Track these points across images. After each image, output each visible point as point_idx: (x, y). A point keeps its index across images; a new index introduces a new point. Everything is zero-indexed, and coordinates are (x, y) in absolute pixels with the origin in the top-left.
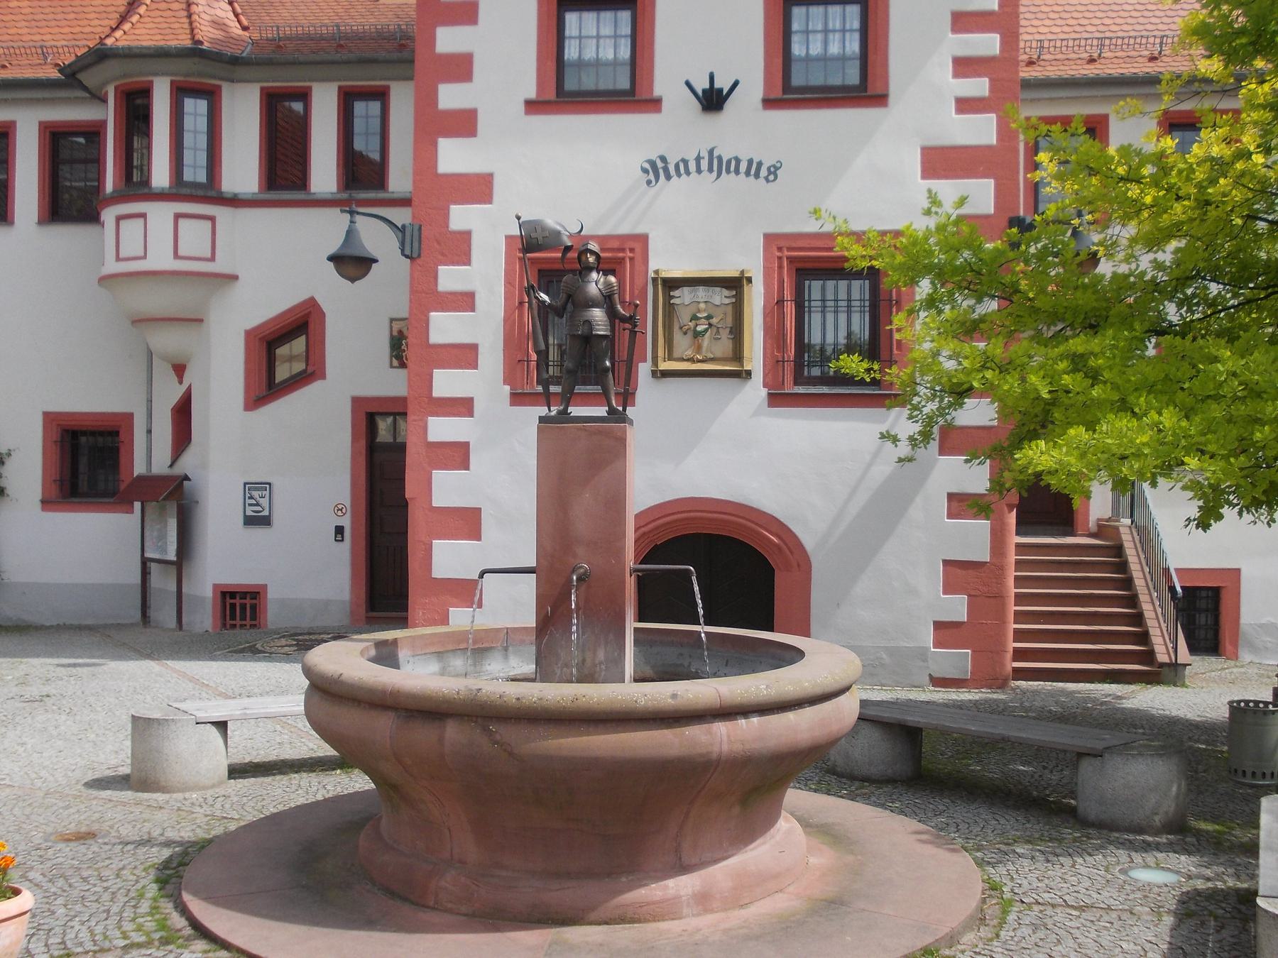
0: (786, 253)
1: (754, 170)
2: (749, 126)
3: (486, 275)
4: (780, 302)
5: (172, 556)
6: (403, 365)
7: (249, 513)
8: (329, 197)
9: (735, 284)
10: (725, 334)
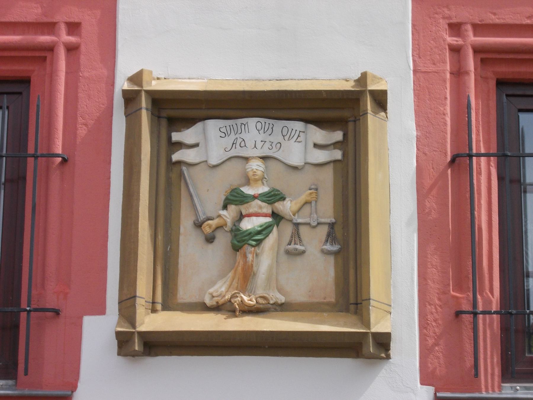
0: (472, 38)
4: (461, 160)
9: (341, 112)
10: (314, 242)
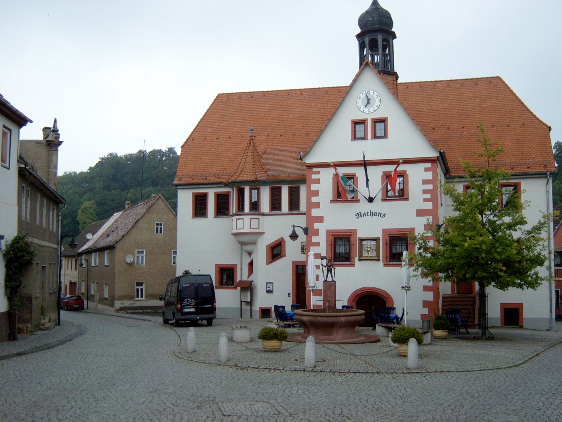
1: (380, 215)
2: (378, 206)
3: (322, 239)
5: (249, 300)
6: (304, 253)
9: (376, 240)
10: (374, 251)
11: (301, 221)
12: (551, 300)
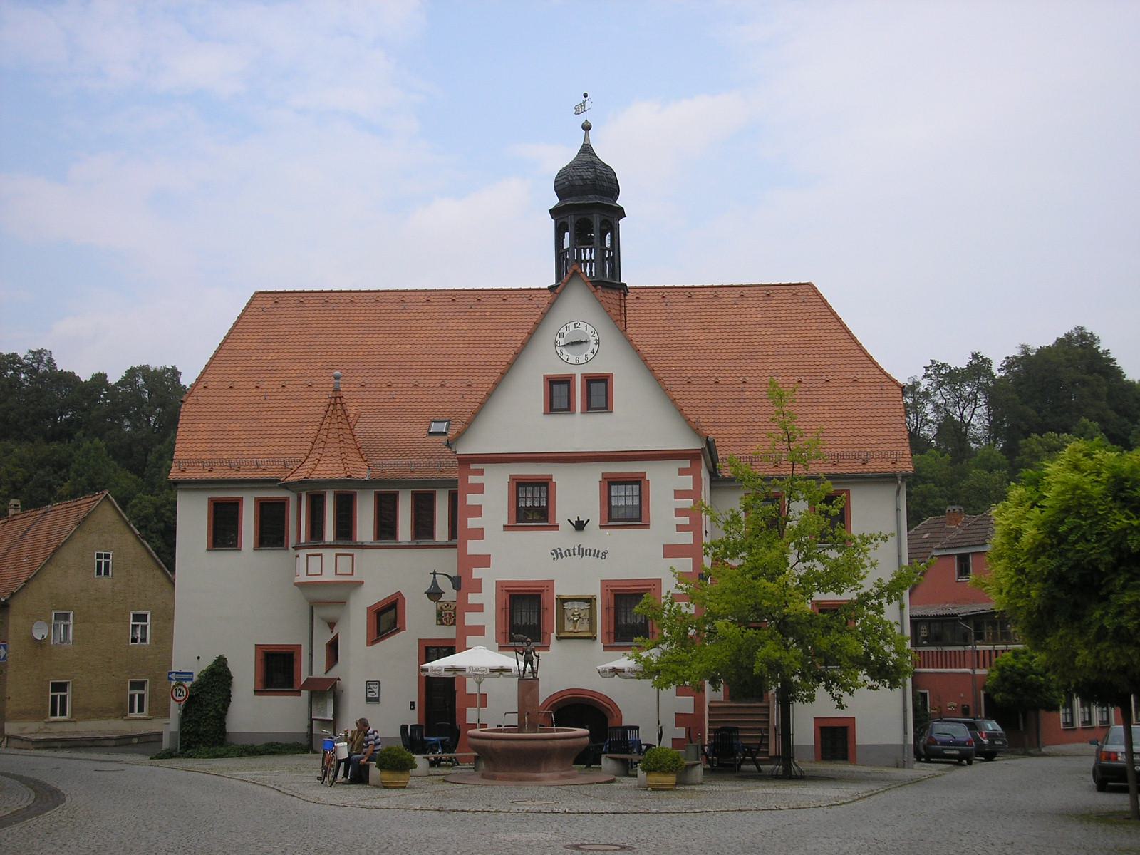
1: (596, 554)
2: (596, 537)
3: (487, 597)
5: (330, 717)
7: (369, 696)
8: (407, 544)
9: (590, 601)
10: (585, 621)
11: (446, 562)
12: (905, 711)
